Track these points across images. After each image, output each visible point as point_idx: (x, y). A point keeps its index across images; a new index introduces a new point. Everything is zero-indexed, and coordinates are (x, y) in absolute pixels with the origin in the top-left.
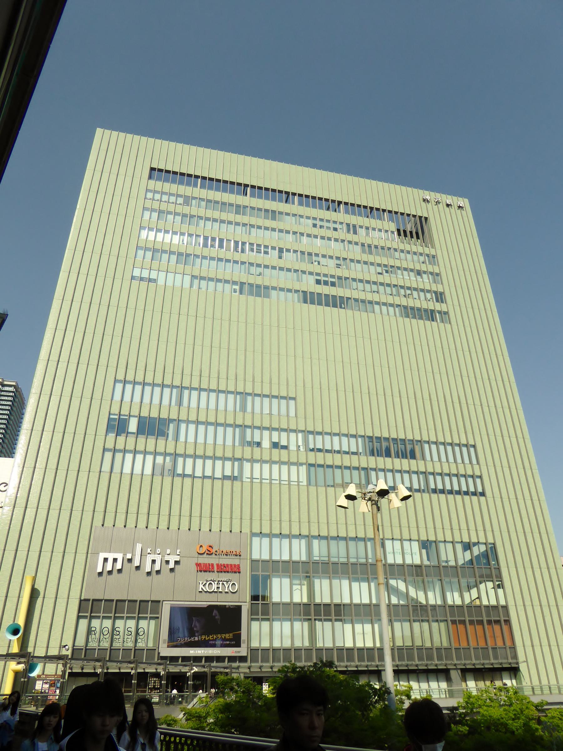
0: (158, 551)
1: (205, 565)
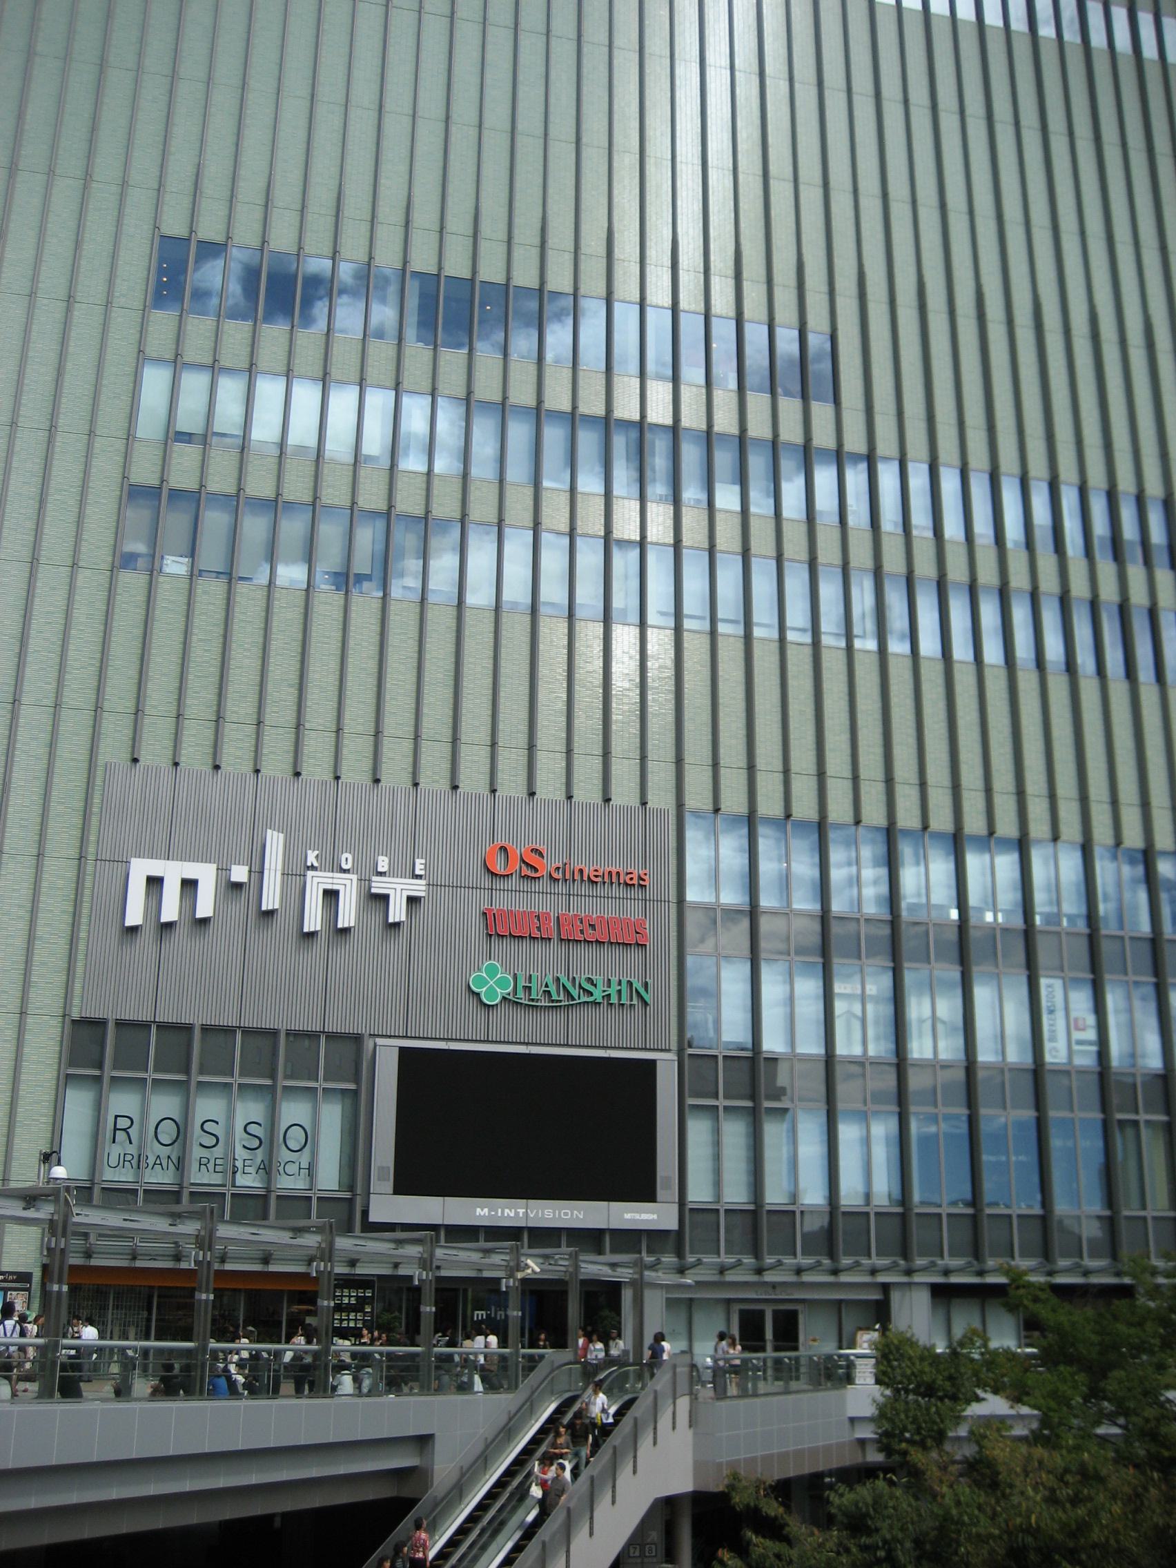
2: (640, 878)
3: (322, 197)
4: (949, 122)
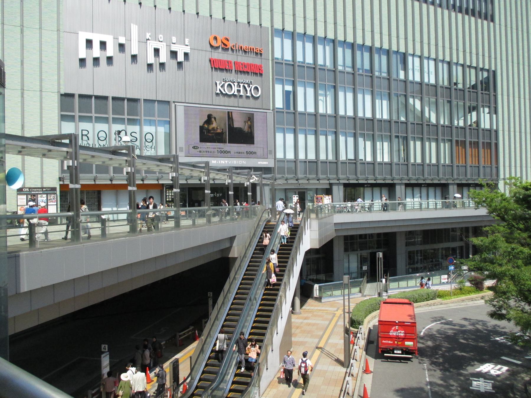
1: (244, 65)
2: (260, 51)
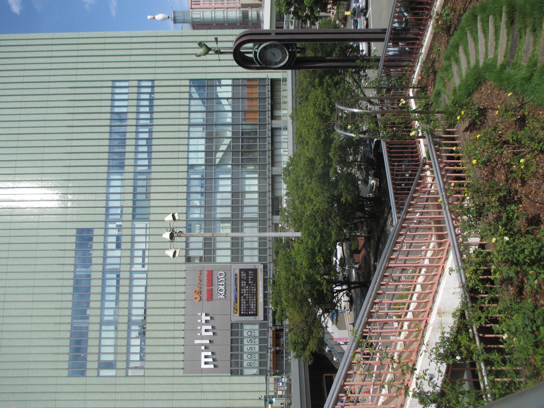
0: (199, 328)
3: (54, 358)
4: (28, 54)
